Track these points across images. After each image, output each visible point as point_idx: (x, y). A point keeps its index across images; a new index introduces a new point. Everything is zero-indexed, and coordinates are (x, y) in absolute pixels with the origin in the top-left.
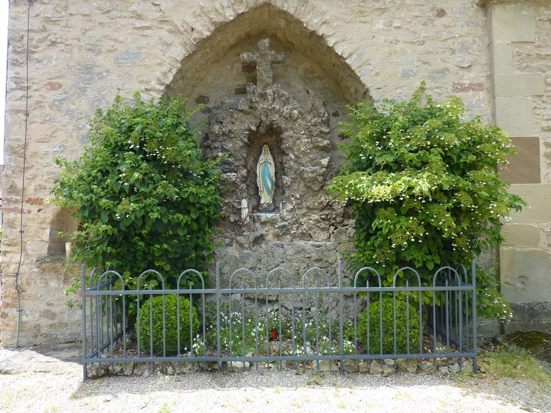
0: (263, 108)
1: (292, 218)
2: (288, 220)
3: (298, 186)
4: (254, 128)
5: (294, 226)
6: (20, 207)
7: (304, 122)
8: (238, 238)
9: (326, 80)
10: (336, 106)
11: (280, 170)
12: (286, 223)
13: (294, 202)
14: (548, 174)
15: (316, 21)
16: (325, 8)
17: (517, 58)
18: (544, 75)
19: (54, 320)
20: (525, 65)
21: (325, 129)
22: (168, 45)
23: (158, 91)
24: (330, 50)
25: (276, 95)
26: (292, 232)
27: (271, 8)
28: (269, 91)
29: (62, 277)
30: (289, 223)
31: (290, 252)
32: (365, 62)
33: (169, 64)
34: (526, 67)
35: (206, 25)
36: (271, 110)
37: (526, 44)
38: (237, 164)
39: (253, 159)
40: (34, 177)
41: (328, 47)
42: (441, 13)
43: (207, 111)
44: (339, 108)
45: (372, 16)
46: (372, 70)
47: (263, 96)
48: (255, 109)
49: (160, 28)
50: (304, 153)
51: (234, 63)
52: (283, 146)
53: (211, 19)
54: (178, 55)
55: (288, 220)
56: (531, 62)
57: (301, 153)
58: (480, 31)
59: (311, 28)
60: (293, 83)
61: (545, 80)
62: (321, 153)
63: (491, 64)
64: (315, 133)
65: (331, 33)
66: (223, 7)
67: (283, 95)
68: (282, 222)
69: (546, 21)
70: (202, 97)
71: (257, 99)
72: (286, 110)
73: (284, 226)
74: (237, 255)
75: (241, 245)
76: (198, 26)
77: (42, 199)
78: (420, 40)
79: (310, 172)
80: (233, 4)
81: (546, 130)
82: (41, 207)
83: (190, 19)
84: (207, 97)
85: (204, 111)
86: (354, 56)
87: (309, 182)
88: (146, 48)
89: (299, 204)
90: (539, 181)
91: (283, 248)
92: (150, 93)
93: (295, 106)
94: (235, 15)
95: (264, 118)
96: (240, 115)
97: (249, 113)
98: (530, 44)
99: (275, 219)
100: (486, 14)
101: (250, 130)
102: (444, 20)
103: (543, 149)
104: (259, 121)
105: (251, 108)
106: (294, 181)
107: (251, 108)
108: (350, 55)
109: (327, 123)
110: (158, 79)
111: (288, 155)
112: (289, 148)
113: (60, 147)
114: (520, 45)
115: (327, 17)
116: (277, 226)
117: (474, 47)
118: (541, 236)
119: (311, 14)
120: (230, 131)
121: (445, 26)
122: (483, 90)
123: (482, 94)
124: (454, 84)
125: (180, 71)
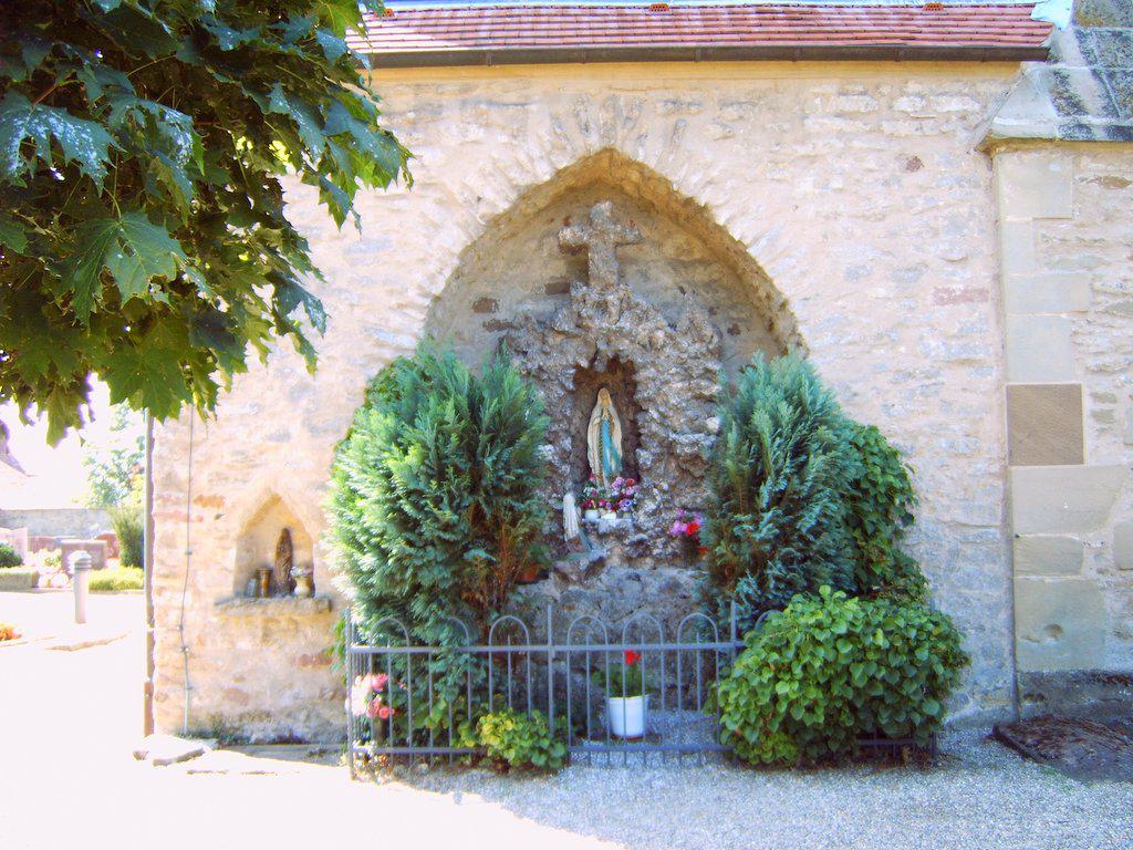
0: (602, 328)
1: (655, 526)
2: (648, 529)
3: (665, 468)
4: (584, 364)
5: (658, 540)
6: (184, 510)
7: (676, 353)
8: (560, 564)
9: (715, 267)
10: (733, 314)
11: (634, 438)
12: (644, 536)
13: (658, 498)
14: (1098, 447)
15: (694, 179)
16: (709, 158)
17: (1044, 246)
18: (1090, 276)
19: (246, 705)
20: (1057, 258)
21: (714, 366)
22: (437, 227)
23: (420, 308)
24: (721, 230)
25: (625, 305)
26: (655, 552)
27: (615, 154)
28: (610, 298)
29: (260, 633)
30: (651, 536)
31: (652, 589)
32: (782, 252)
33: (439, 260)
34: (1059, 262)
35: (503, 191)
36: (615, 332)
37: (1060, 222)
38: (553, 429)
39: (581, 415)
40: (209, 459)
41: (717, 226)
42: (914, 164)
43: (498, 326)
44: (739, 319)
45: (792, 169)
46: (794, 267)
47: (602, 307)
48: (587, 329)
49: (422, 197)
50: (677, 409)
51: (544, 237)
52: (638, 396)
53: (510, 181)
54: (454, 245)
55: (648, 529)
56: (1068, 252)
57: (670, 409)
58: (980, 197)
59: (686, 193)
60: (653, 272)
61: (1091, 285)
62: (707, 406)
63: (997, 256)
64: (695, 373)
65: (721, 201)
66: (531, 160)
67: (637, 305)
68: (636, 533)
69: (1092, 181)
70: (486, 300)
71: (591, 312)
72: (642, 332)
73: (641, 542)
74: (557, 595)
75: (565, 577)
76: (489, 194)
77: (222, 498)
78: (877, 211)
79: (687, 445)
80: (549, 153)
81: (1093, 372)
82: (221, 511)
83: (473, 181)
84: (495, 301)
85: (490, 327)
86: (763, 242)
87: (685, 462)
88: (398, 232)
89: (668, 501)
90: (1080, 460)
91: (639, 580)
92: (405, 310)
93: (659, 325)
94: (553, 172)
95: (602, 347)
96: (559, 339)
97: (575, 336)
98: (1064, 221)
99: (623, 529)
100: (991, 167)
101: (577, 367)
102: (918, 177)
103: (1088, 404)
104: (593, 350)
105: (578, 326)
106: (658, 458)
107: (578, 326)
108: (756, 240)
109: (719, 353)
110: (420, 287)
111: (646, 411)
112: (650, 400)
113: (252, 406)
114: (1048, 223)
115: (714, 173)
116: (627, 542)
117: (971, 224)
118: (1085, 556)
119: (686, 166)
120: (540, 368)
121: (921, 187)
122: (987, 300)
123: (985, 308)
124: (938, 291)
125: (458, 274)
